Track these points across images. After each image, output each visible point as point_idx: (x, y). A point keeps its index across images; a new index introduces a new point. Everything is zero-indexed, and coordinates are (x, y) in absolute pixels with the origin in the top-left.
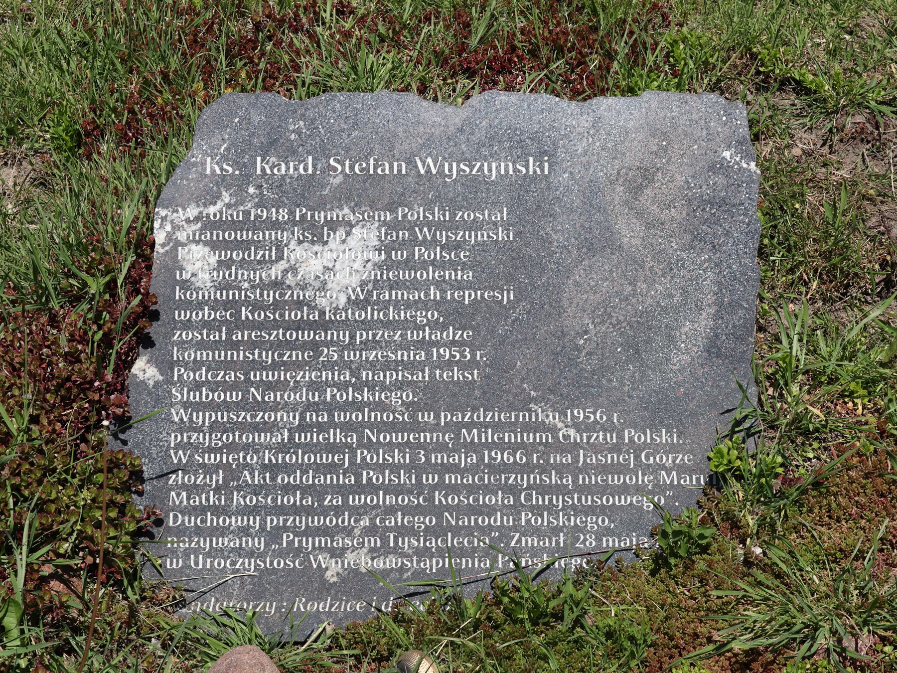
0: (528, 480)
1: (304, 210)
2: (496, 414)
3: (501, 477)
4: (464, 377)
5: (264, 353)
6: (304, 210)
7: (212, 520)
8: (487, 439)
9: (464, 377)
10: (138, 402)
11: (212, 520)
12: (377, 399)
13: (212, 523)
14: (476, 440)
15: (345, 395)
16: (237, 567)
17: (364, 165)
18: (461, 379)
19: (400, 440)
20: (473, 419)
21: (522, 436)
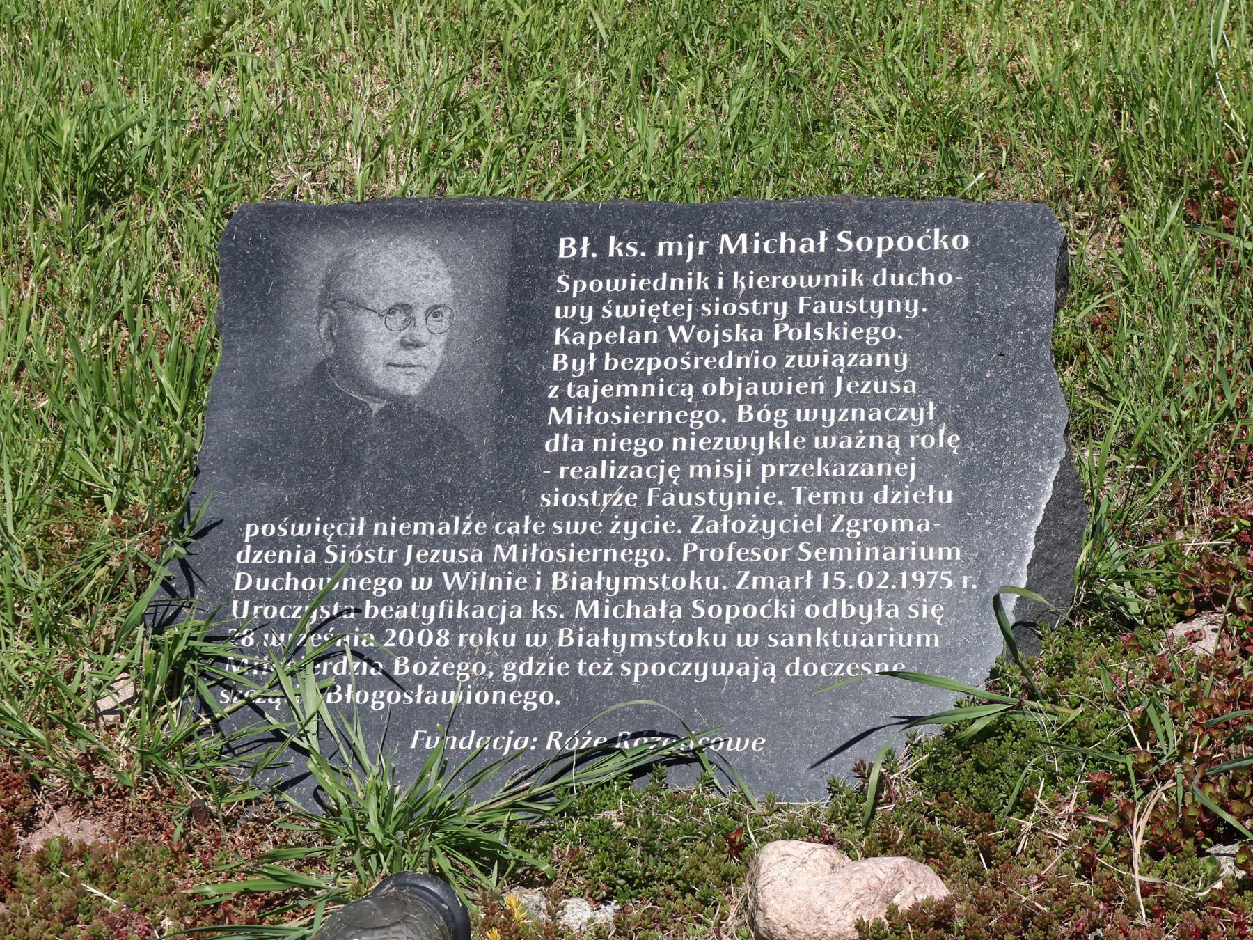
0: (621, 585)
1: (695, 547)
2: (907, 493)
3: (822, 495)
4: (547, 613)
5: (722, 495)
6: (695, 547)
7: (292, 582)
8: (529, 557)
9: (547, 613)
10: (862, 869)
11: (292, 582)
12: (845, 337)
13: (292, 587)
14: (514, 559)
15: (800, 332)
16: (294, 616)
17: (819, 495)
18: (542, 616)
19: (576, 531)
20: (441, 672)
21: (896, 638)
